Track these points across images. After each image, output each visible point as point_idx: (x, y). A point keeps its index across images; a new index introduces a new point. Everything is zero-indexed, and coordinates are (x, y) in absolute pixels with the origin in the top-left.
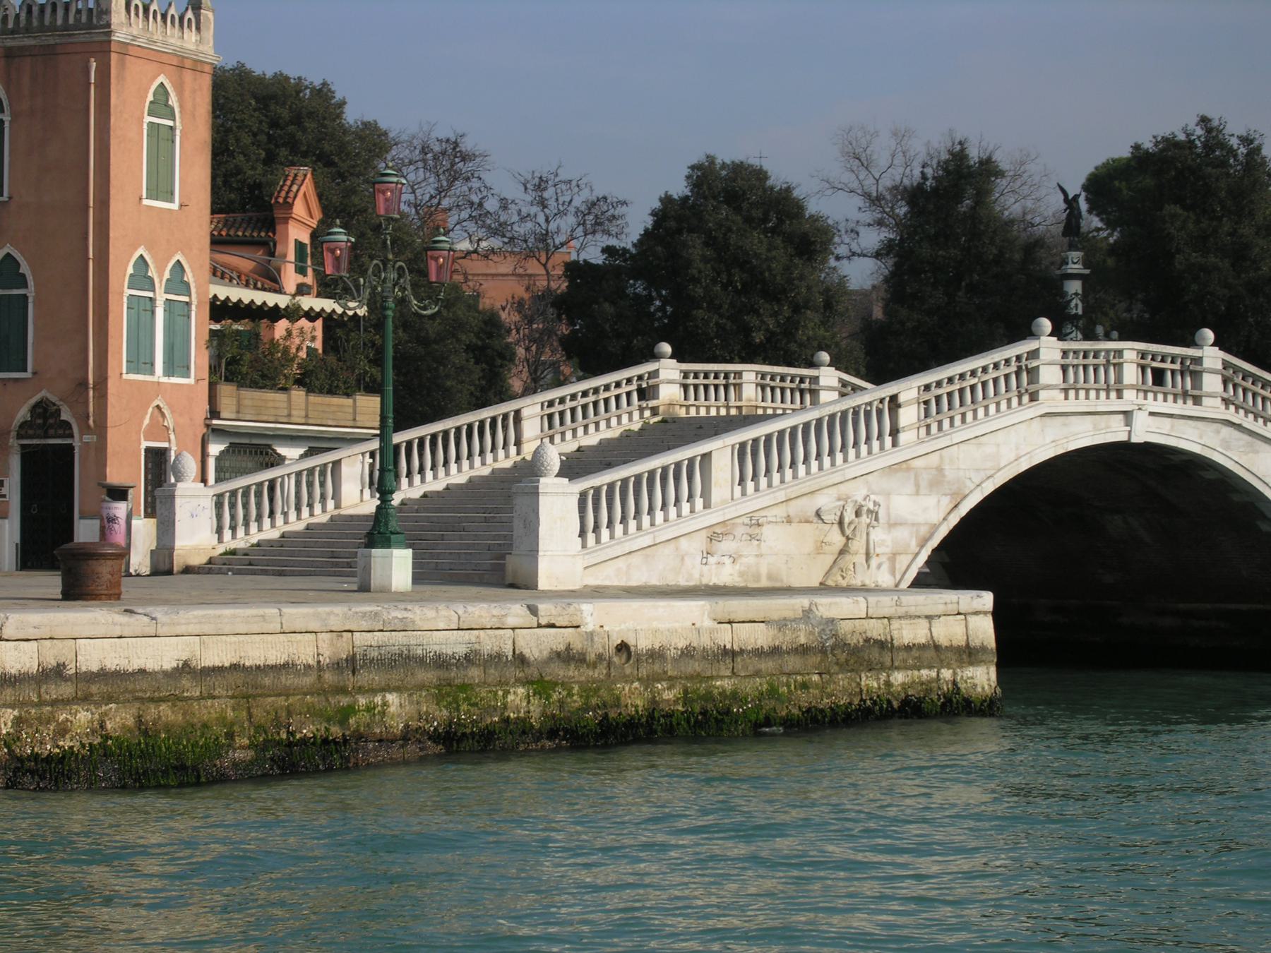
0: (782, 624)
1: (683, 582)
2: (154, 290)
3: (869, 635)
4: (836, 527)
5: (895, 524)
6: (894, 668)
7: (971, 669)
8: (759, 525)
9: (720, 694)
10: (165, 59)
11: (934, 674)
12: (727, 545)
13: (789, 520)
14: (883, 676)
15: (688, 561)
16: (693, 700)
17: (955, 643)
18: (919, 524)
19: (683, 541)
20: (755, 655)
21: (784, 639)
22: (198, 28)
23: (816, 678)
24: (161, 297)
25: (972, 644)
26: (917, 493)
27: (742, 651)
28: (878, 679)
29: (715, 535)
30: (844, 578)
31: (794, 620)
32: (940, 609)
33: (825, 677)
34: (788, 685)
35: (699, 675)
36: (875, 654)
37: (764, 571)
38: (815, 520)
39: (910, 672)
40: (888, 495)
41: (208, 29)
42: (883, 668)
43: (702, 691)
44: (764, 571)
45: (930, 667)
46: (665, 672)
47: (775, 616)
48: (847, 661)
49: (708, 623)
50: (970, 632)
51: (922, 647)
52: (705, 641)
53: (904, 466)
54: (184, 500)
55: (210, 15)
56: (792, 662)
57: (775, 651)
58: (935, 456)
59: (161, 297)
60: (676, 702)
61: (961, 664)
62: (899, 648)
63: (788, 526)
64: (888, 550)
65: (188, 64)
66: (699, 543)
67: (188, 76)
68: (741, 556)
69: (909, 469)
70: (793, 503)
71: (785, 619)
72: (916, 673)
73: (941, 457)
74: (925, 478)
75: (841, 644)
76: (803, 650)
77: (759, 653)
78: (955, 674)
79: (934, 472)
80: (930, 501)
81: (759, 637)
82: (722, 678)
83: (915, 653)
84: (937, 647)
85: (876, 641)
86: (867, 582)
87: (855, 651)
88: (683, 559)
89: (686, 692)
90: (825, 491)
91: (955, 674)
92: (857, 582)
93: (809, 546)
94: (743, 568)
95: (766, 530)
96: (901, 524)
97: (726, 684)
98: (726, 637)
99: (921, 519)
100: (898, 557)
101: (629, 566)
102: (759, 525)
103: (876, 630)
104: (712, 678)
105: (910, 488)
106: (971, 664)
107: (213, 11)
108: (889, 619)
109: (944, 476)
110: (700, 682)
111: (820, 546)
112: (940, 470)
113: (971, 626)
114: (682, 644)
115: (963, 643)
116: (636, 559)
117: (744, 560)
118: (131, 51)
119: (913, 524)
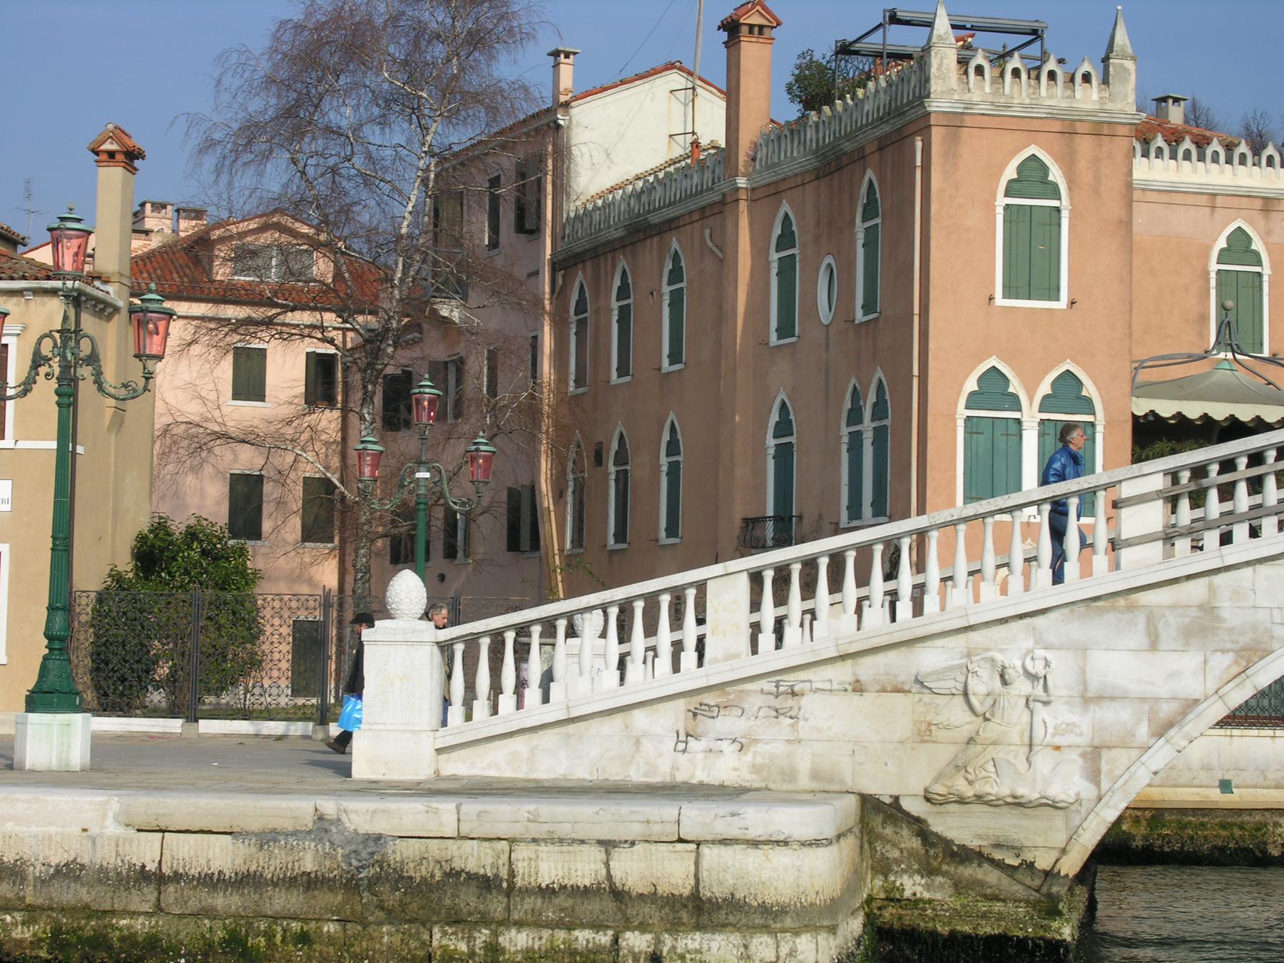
0: (267, 838)
1: (636, 776)
2: (1020, 410)
3: (457, 865)
4: (959, 700)
5: (1100, 698)
6: (506, 923)
7: (698, 936)
8: (793, 694)
9: (122, 939)
10: (1035, 125)
11: (605, 939)
12: (728, 724)
13: (858, 688)
14: (482, 936)
15: (647, 745)
16: (69, 944)
17: (663, 889)
18: (1157, 700)
19: (638, 714)
20: (205, 884)
21: (274, 862)
22: (1105, 81)
23: (330, 928)
24: (1031, 417)
25: (705, 893)
26: (1153, 646)
27: (177, 877)
28: (471, 939)
29: (703, 704)
30: (970, 783)
31: (295, 833)
32: (634, 831)
33: (353, 928)
34: (269, 935)
35: (86, 907)
36: (468, 899)
37: (804, 767)
38: (916, 688)
39: (546, 934)
40: (1082, 650)
41: (1126, 81)
42: (485, 920)
43: (88, 932)
44: (804, 767)
45: (597, 927)
46: (22, 899)
47: (255, 826)
48: (403, 905)
49: (112, 829)
50: (704, 874)
51: (585, 892)
52: (106, 856)
53: (1121, 602)
54: (373, 648)
55: (1130, 65)
56: (280, 901)
57: (245, 881)
58: (1199, 586)
59: (1031, 417)
60: (37, 942)
61: (675, 927)
62: (527, 891)
63: (856, 698)
64: (1084, 740)
65: (1080, 128)
66: (673, 716)
67: (1085, 145)
68: (756, 741)
69: (1131, 608)
70: (868, 661)
71: (274, 831)
72: (561, 935)
73: (1212, 589)
74: (1170, 626)
75: (399, 879)
76: (311, 882)
77: (212, 882)
78: (658, 941)
79: (1194, 613)
80: (1189, 661)
81: (221, 856)
82: (134, 914)
83: (560, 900)
84: (619, 895)
85: (471, 877)
86: (1021, 791)
87: (424, 889)
88: (638, 742)
89: (57, 931)
90: (939, 642)
91: (658, 941)
92: (999, 788)
93: (903, 727)
94: (759, 760)
95: (811, 705)
96: (1112, 698)
97: (141, 925)
98: (146, 852)
99: (1162, 690)
100: (1105, 754)
101: (533, 750)
102: (793, 694)
103: (476, 858)
104: (113, 912)
105: (1138, 637)
106: (699, 927)
107: (1133, 58)
108: (512, 841)
109: (1218, 619)
110: (89, 917)
111: (925, 733)
112: (1209, 609)
113: (705, 864)
114: (57, 858)
115: (686, 892)
116: (547, 739)
117: (762, 748)
118: (968, 121)
119: (1143, 700)
